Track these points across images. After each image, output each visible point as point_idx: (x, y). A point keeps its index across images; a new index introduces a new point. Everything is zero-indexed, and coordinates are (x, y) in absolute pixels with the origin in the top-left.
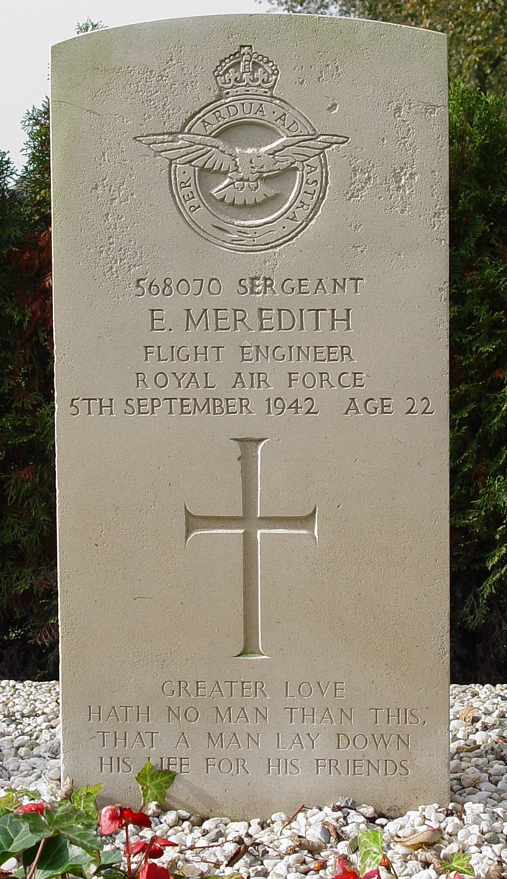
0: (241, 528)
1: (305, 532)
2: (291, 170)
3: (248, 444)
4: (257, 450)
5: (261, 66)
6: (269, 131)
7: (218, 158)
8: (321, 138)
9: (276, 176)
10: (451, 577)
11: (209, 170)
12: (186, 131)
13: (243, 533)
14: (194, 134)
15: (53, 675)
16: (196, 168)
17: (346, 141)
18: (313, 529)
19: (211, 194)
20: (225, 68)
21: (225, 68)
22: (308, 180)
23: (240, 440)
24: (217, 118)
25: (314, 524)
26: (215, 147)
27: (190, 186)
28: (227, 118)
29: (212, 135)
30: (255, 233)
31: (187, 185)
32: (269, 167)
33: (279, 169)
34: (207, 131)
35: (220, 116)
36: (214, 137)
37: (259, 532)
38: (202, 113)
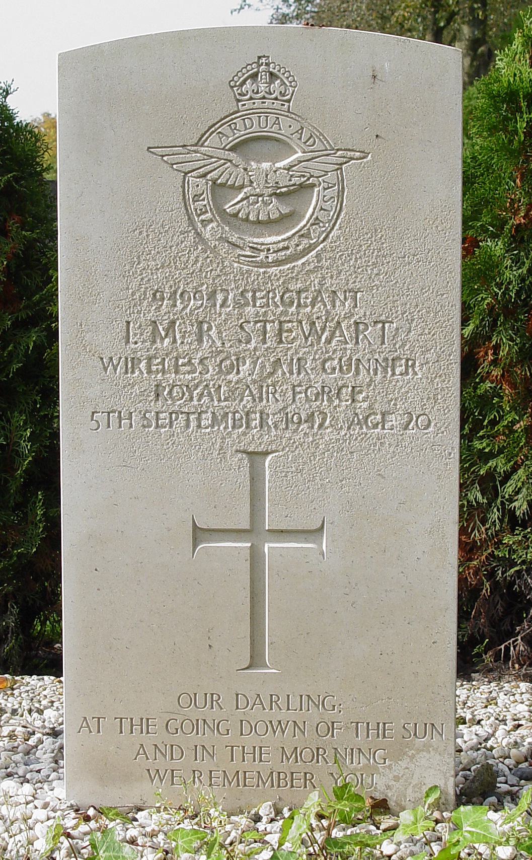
0: (245, 541)
2: (304, 188)
3: (255, 456)
4: (266, 459)
5: (277, 77)
7: (231, 175)
8: (339, 153)
9: (294, 191)
11: (223, 185)
13: (250, 547)
14: (207, 147)
18: (322, 543)
20: (242, 79)
21: (242, 79)
22: (324, 196)
24: (233, 130)
25: (322, 539)
27: (203, 200)
28: (241, 134)
29: (227, 148)
34: (222, 144)
35: (235, 129)
36: (229, 150)
37: (266, 545)
38: (217, 126)
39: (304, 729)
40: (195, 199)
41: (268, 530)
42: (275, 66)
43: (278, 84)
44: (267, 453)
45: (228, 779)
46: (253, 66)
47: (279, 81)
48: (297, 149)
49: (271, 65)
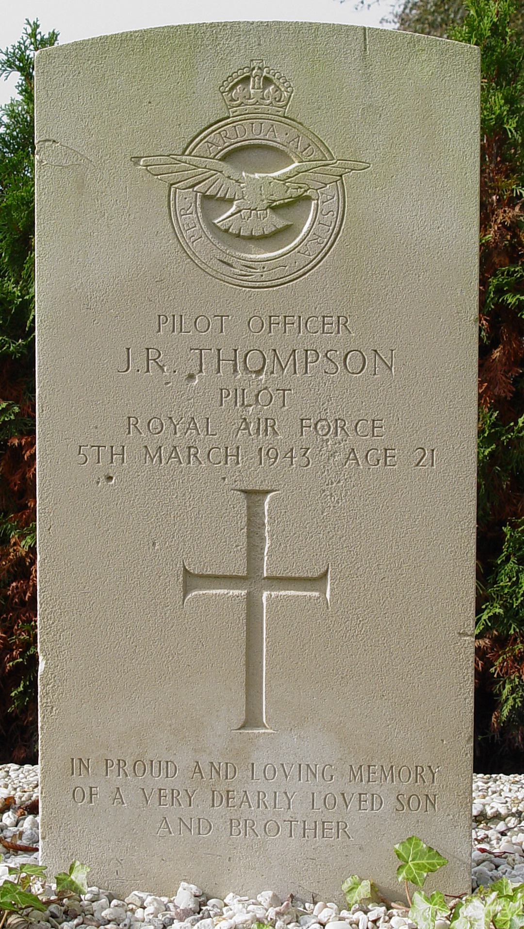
1: (317, 594)
2: (303, 200)
3: (254, 496)
4: (264, 501)
6: (279, 155)
10: (478, 535)
12: (187, 153)
15: (33, 760)
16: (198, 194)
17: (368, 167)
19: (214, 224)
23: (244, 491)
26: (220, 172)
30: (264, 268)
31: (188, 212)
32: (280, 196)
33: (291, 198)
34: (210, 154)
36: (220, 160)
37: (265, 594)
39: (191, 827)
40: (182, 213)
41: (268, 578)
42: (270, 70)
43: (272, 89)
44: (268, 492)
45: (353, 773)
46: (245, 70)
47: (273, 87)
48: (294, 159)
49: (265, 70)
